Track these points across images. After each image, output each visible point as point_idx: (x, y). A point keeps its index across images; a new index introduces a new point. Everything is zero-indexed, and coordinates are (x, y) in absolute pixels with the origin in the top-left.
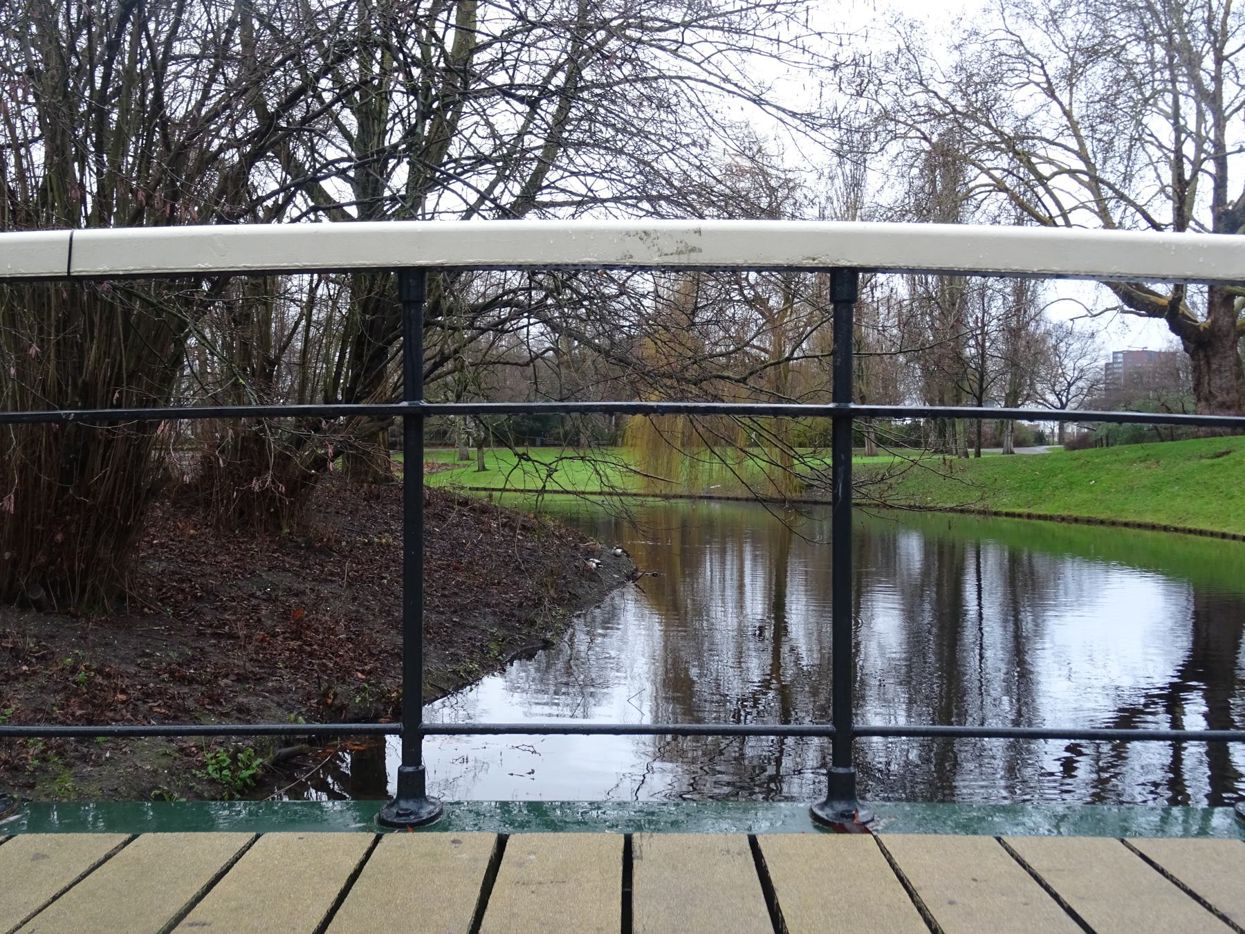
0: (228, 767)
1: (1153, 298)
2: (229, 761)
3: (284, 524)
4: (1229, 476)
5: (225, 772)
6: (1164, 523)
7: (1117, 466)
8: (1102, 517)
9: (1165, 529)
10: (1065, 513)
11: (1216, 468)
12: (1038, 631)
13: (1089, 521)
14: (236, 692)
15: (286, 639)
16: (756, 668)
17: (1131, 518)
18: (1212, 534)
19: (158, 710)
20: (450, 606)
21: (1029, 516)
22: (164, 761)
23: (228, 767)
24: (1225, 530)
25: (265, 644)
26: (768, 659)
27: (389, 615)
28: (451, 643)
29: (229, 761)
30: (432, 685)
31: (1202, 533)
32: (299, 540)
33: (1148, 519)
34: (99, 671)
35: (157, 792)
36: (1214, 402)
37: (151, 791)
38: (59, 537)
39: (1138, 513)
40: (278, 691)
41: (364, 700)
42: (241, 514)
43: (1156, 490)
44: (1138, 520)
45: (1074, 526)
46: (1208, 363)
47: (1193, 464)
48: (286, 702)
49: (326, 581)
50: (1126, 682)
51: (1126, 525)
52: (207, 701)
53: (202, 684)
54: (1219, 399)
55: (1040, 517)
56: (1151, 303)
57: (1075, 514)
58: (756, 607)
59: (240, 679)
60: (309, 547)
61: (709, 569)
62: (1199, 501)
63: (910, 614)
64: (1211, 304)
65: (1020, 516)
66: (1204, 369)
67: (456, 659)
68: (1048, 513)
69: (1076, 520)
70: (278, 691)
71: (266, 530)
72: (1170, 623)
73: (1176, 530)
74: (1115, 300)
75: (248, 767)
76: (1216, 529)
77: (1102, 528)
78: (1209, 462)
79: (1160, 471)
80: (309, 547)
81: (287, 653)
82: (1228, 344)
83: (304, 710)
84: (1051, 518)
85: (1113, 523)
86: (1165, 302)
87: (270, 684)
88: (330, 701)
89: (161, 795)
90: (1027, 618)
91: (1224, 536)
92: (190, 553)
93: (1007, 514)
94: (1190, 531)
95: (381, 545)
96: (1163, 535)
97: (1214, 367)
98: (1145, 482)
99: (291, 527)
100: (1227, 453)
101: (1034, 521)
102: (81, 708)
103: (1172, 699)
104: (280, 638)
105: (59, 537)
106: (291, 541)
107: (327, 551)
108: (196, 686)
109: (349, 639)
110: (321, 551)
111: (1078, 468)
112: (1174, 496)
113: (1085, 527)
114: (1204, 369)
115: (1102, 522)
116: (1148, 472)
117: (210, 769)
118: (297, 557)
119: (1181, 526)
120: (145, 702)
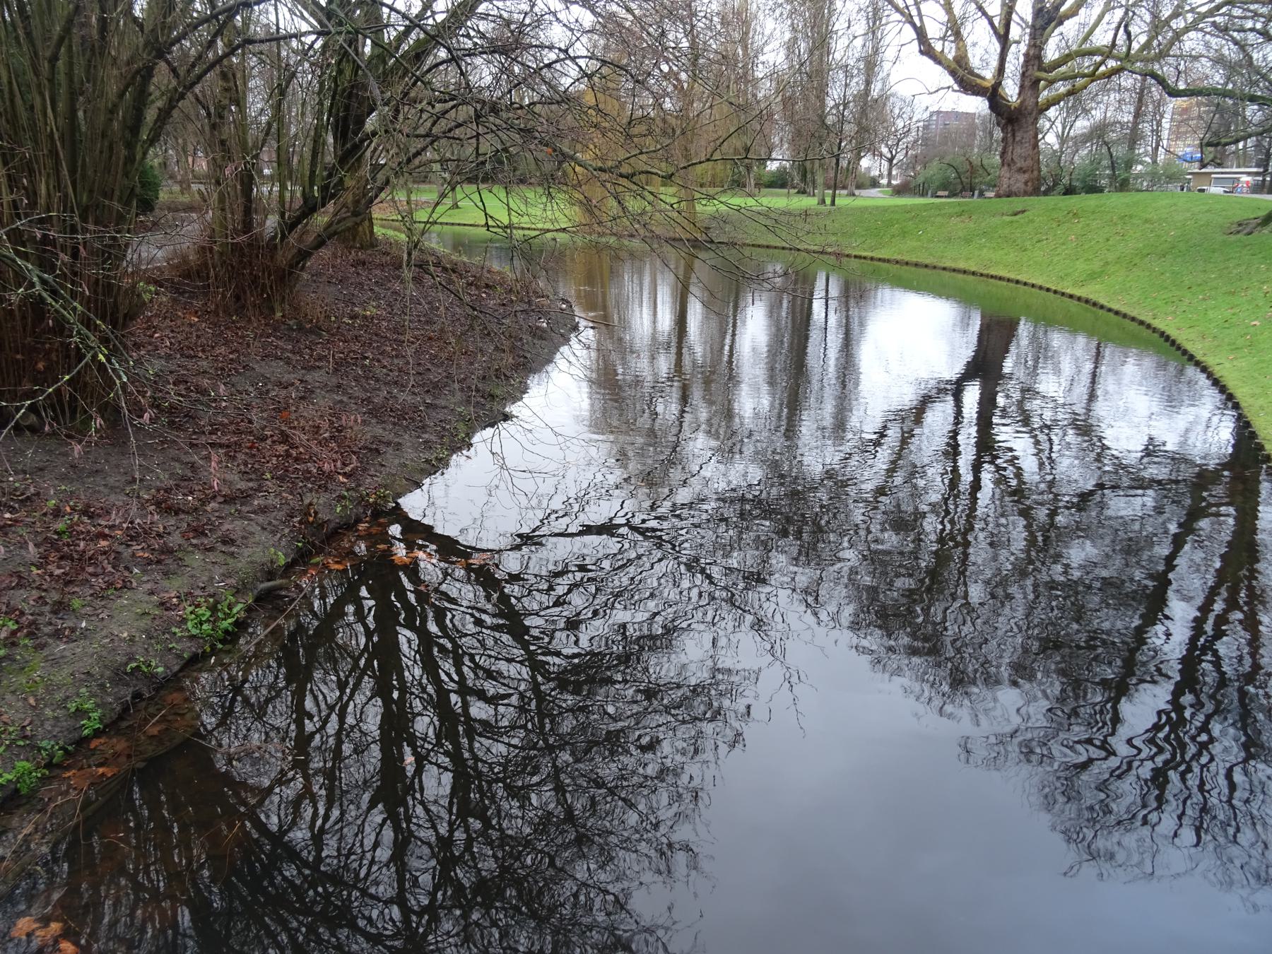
0: (208, 621)
1: (979, 81)
2: (208, 613)
3: (277, 306)
4: (1024, 232)
5: (205, 627)
6: (973, 269)
7: (939, 219)
8: (927, 262)
9: (974, 273)
10: (899, 257)
11: (1015, 225)
12: (862, 324)
13: (916, 265)
14: (222, 518)
15: (274, 442)
16: (664, 364)
17: (948, 264)
18: (1009, 280)
19: (141, 554)
20: (423, 385)
21: (872, 259)
22: (145, 622)
23: (208, 621)
24: (1019, 277)
25: (254, 451)
26: (673, 357)
27: (369, 402)
28: (424, 428)
29: (208, 613)
30: (407, 480)
31: (1001, 278)
32: (291, 323)
33: (961, 265)
34: (85, 512)
35: (134, 665)
36: (1014, 168)
37: (127, 664)
38: (41, 366)
39: (954, 260)
40: (263, 510)
41: (344, 507)
42: (238, 298)
43: (968, 241)
44: (953, 265)
45: (905, 267)
46: (1014, 135)
47: (996, 220)
48: (270, 523)
49: (314, 368)
50: (925, 375)
51: (944, 269)
52: (191, 535)
53: (188, 513)
54: (1019, 165)
55: (880, 260)
56: (977, 85)
57: (907, 258)
58: (666, 320)
59: (229, 500)
60: (301, 328)
61: (628, 282)
62: (1001, 252)
63: (773, 312)
64: (1022, 87)
65: (865, 258)
66: (1010, 140)
67: (428, 445)
68: (886, 257)
69: (907, 263)
70: (263, 510)
71: (261, 313)
72: (951, 322)
73: (982, 275)
74: (950, 81)
75: (227, 616)
76: (1012, 276)
77: (925, 270)
78: (1008, 219)
79: (972, 225)
80: (301, 328)
81: (274, 460)
82: (1030, 120)
83: (287, 531)
84: (888, 261)
85: (935, 267)
86: (988, 84)
87: (256, 503)
88: (311, 519)
89: (138, 667)
90: (854, 312)
91: (1018, 282)
92: (189, 348)
93: (856, 257)
94: (992, 277)
95: (365, 317)
96: (971, 278)
97: (1018, 139)
98: (960, 234)
99: (283, 310)
100: (1023, 212)
101: (876, 263)
102: (59, 567)
103: (957, 390)
104: (269, 442)
105: (41, 366)
106: (284, 323)
107: (316, 330)
108: (182, 516)
109: (333, 437)
110: (311, 331)
111: (911, 219)
112: (981, 248)
113: (913, 269)
114: (1010, 140)
115: (926, 266)
116: (963, 225)
117: (190, 625)
118: (290, 339)
119: (985, 272)
120: (128, 546)
